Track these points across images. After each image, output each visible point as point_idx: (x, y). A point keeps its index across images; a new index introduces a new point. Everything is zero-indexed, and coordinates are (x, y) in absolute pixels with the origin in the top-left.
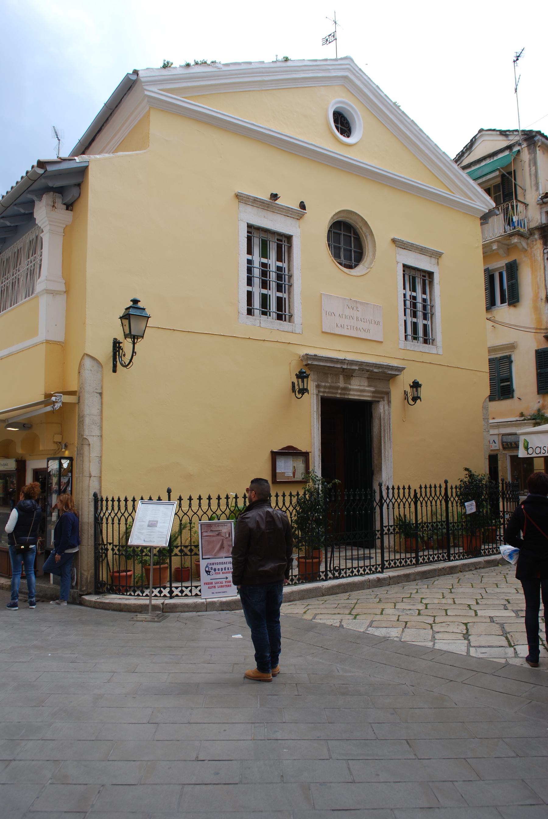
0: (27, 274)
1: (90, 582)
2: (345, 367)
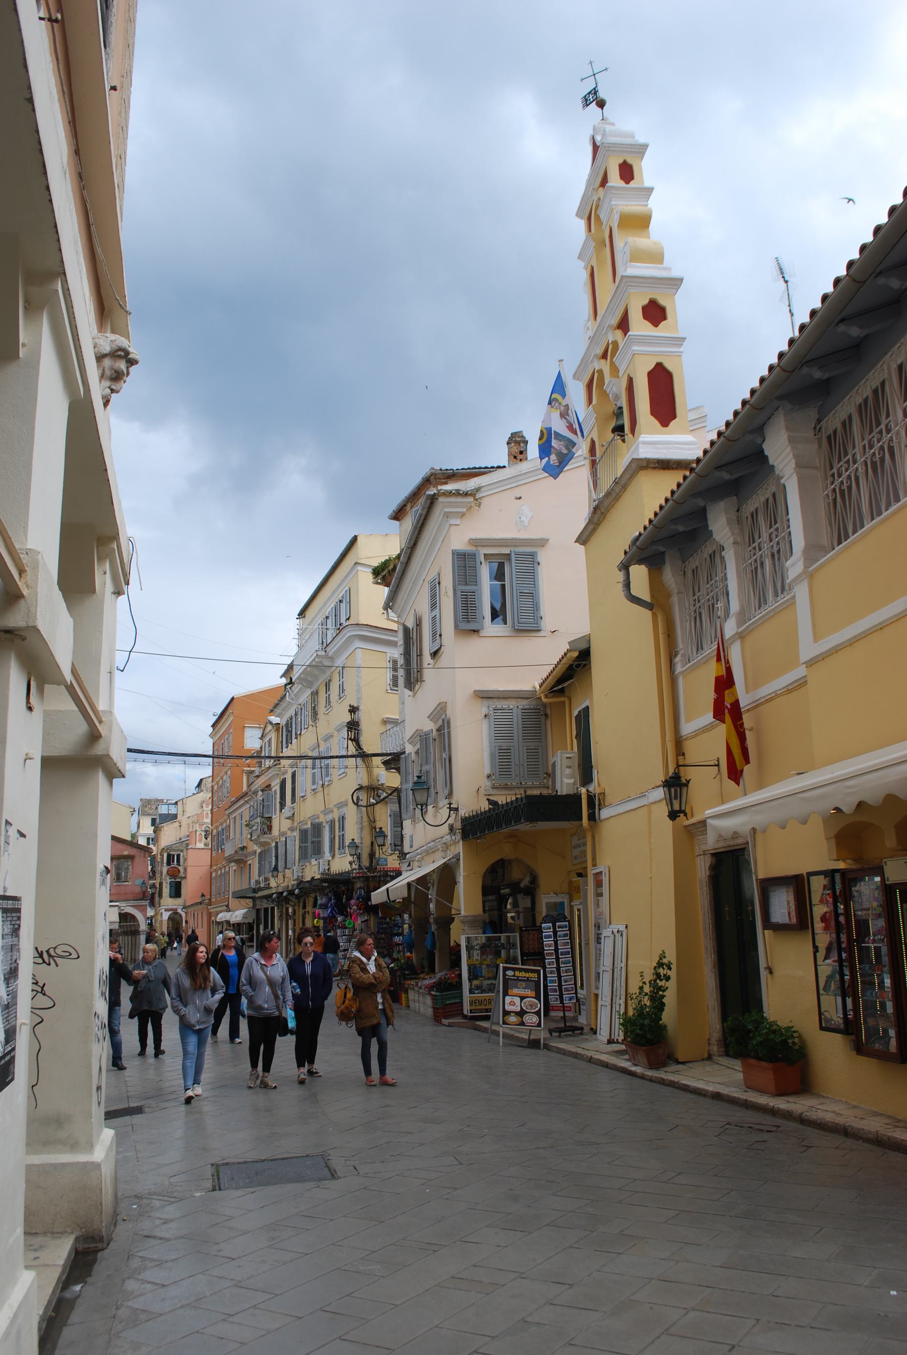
0: (835, 500)
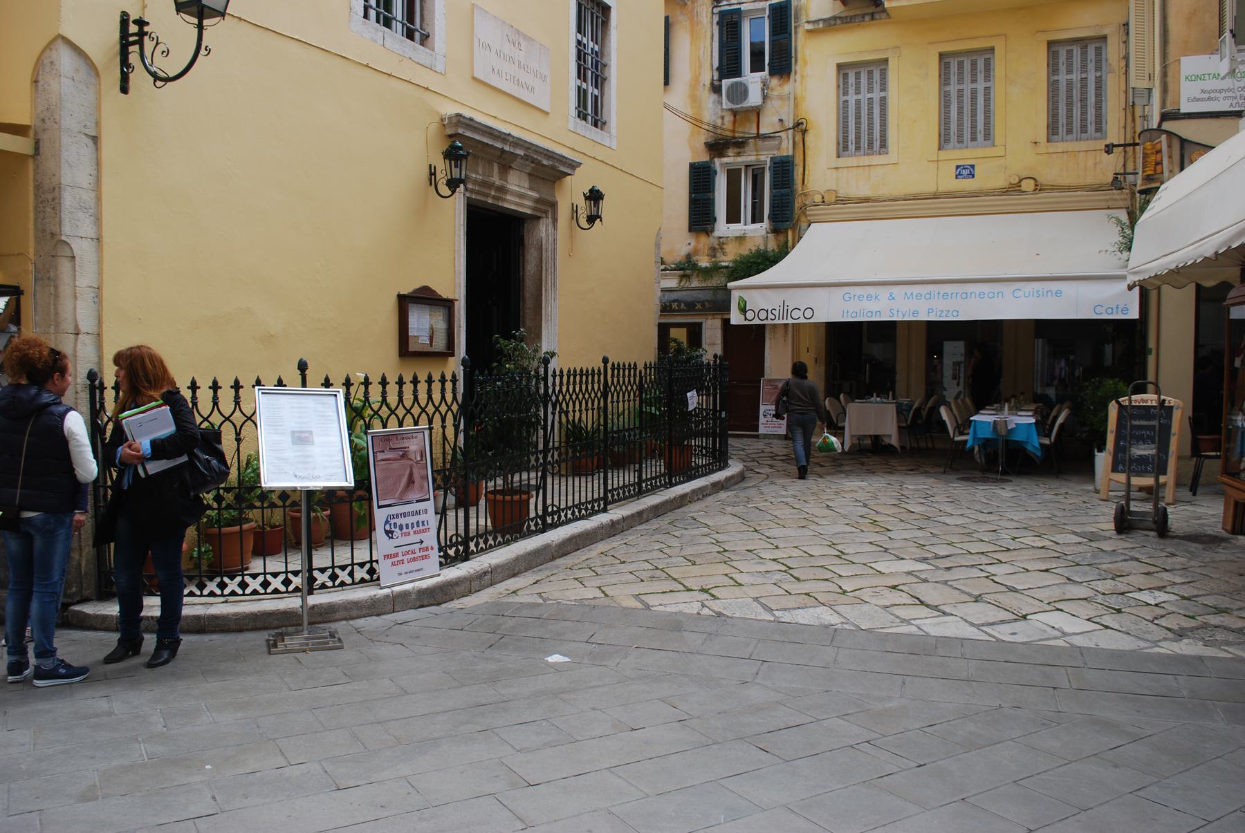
1: (86, 573)
2: (507, 148)
